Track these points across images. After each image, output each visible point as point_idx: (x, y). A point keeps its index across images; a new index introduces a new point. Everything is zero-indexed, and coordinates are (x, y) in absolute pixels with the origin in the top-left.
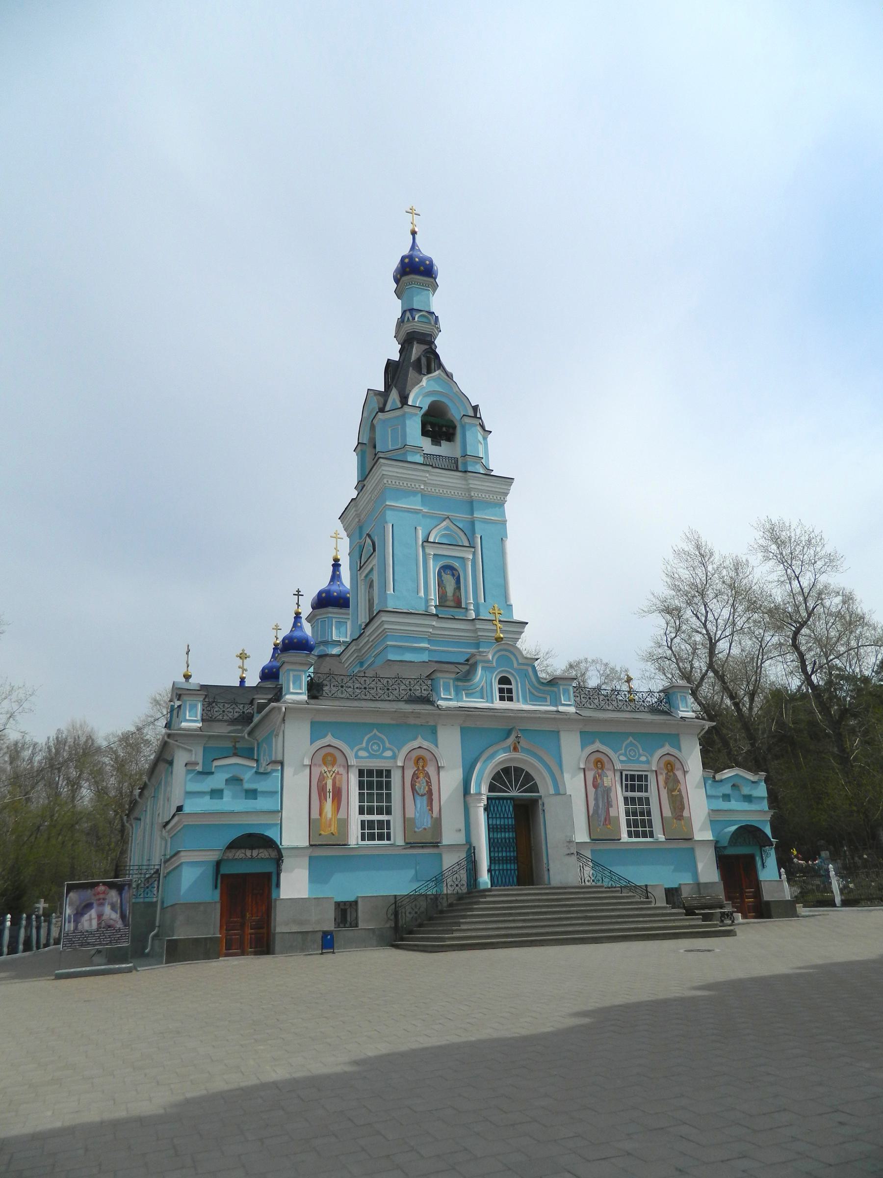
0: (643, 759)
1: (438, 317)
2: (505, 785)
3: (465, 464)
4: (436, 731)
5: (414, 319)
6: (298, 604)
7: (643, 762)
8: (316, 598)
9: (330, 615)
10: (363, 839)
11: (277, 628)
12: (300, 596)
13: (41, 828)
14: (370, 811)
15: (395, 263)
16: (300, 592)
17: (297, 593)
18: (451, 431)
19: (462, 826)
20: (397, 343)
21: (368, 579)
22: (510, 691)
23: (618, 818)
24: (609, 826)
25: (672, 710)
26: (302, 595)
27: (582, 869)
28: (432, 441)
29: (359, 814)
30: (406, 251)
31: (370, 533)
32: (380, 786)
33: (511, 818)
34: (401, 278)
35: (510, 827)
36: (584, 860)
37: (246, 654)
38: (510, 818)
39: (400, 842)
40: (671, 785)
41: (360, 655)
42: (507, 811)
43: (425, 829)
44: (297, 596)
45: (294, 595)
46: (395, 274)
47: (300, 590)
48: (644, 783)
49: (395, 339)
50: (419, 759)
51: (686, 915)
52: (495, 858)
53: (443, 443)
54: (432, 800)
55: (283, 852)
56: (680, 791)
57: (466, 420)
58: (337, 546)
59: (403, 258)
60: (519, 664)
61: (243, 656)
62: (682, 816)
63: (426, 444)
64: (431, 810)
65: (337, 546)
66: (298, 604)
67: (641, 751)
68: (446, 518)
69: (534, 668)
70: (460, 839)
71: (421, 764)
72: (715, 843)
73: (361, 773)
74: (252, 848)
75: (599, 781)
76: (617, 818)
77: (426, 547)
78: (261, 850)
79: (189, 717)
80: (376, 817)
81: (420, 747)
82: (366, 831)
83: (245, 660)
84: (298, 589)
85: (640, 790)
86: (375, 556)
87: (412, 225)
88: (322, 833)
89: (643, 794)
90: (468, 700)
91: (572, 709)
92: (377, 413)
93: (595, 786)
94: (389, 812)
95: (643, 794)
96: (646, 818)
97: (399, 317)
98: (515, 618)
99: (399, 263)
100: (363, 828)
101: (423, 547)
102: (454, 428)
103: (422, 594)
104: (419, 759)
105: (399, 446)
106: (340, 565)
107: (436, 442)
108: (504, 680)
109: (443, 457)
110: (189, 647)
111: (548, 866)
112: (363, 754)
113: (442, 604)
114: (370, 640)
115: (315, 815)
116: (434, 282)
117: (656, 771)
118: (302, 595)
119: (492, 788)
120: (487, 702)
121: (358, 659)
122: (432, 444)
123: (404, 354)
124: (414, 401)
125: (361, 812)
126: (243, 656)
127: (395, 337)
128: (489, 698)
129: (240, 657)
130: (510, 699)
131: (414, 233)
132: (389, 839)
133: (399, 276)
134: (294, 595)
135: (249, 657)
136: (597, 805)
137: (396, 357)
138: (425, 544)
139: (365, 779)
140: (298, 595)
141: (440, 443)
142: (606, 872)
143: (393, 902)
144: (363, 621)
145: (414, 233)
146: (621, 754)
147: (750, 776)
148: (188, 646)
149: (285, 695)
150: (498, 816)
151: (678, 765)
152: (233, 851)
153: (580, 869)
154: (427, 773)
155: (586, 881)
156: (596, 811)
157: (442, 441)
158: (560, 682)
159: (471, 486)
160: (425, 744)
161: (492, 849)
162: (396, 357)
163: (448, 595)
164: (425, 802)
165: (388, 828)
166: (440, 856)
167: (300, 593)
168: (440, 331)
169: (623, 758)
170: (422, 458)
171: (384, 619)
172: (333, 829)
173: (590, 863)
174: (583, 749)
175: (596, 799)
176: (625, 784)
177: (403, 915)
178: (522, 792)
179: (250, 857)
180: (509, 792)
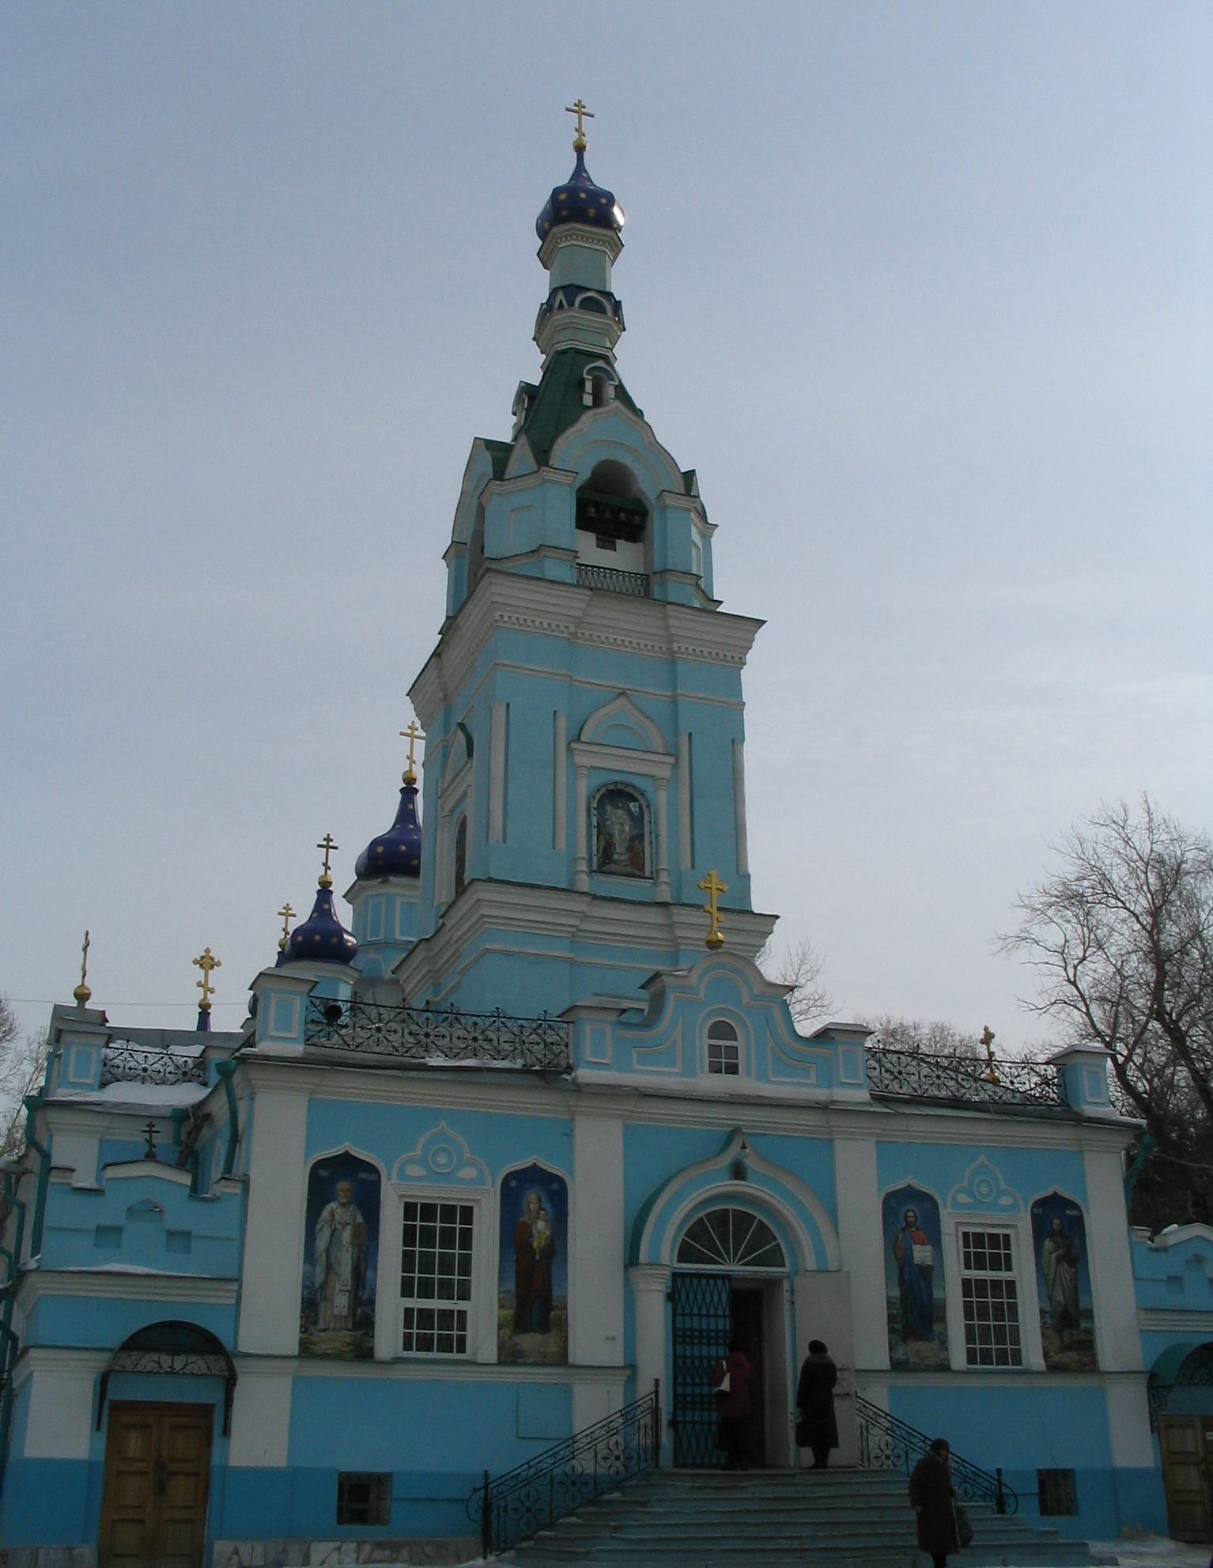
1: (620, 302)
2: (718, 1252)
4: (572, 1130)
6: (325, 864)
8: (366, 854)
10: (407, 1346)
11: (287, 913)
12: (330, 850)
14: (426, 1292)
15: (540, 201)
16: (332, 840)
19: (618, 1331)
20: (539, 350)
21: (457, 813)
22: (733, 1052)
26: (336, 848)
27: (865, 1433)
28: (597, 539)
29: (402, 1296)
30: (563, 180)
31: (465, 722)
32: (448, 1239)
33: (724, 1316)
34: (550, 228)
35: (721, 1334)
36: (871, 1413)
37: (212, 959)
38: (722, 1316)
42: (708, 1301)
44: (325, 849)
46: (539, 221)
47: (331, 837)
48: (1002, 1251)
49: (535, 343)
52: (685, 1399)
53: (620, 543)
55: (237, 1363)
57: (670, 500)
58: (411, 752)
59: (556, 192)
61: (207, 962)
63: (587, 546)
65: (411, 752)
67: (1003, 1185)
68: (621, 694)
69: (785, 1006)
74: (174, 1351)
77: (574, 752)
78: (193, 1358)
80: (435, 1304)
82: (415, 1331)
83: (210, 972)
84: (328, 835)
85: (996, 1267)
86: (471, 767)
87: (577, 133)
89: (1002, 1275)
90: (643, 1068)
92: (490, 480)
94: (465, 1295)
95: (1002, 1275)
96: (1007, 1323)
97: (545, 301)
99: (548, 202)
100: (408, 1323)
107: (606, 540)
108: (722, 1030)
109: (618, 571)
110: (89, 937)
112: (414, 1170)
114: (454, 939)
116: (615, 237)
118: (336, 848)
119: (685, 1254)
121: (430, 978)
122: (598, 546)
123: (548, 374)
125: (407, 1290)
126: (207, 962)
127: (534, 339)
129: (201, 965)
130: (733, 1069)
131: (580, 149)
132: (462, 1348)
133: (546, 225)
135: (218, 964)
137: (535, 378)
138: (574, 746)
139: (418, 1223)
141: (614, 544)
142: (914, 1440)
143: (482, 1485)
144: (443, 900)
145: (580, 149)
146: (411, 1161)
148: (87, 934)
149: (261, 1039)
150: (695, 1311)
152: (135, 1355)
153: (861, 1433)
155: (872, 1459)
157: (618, 541)
158: (838, 1037)
159: (673, 631)
161: (680, 1380)
162: (535, 378)
165: (462, 1326)
166: (568, 1390)
168: (624, 329)
170: (575, 573)
171: (482, 895)
173: (882, 1420)
176: (965, 1252)
177: (502, 1514)
179: (169, 1370)
180: (721, 1264)
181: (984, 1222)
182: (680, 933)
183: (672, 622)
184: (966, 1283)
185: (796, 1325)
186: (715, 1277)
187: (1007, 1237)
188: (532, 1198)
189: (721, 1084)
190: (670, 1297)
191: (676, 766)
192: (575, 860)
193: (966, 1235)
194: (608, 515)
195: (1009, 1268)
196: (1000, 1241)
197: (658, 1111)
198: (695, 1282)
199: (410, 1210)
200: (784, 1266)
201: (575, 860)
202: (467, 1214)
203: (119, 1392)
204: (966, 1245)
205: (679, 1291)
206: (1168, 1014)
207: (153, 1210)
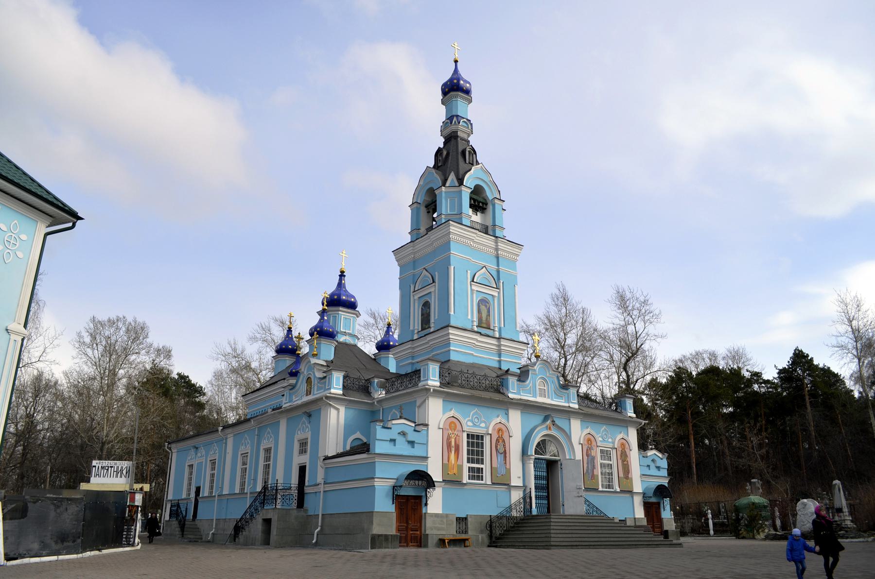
3: (494, 231)
5: (459, 123)
9: (340, 313)
10: (469, 479)
13: (771, 499)
18: (485, 206)
19: (521, 475)
23: (598, 476)
25: (623, 411)
39: (489, 482)
40: (623, 457)
41: (413, 351)
43: (502, 475)
46: (443, 87)
50: (499, 430)
54: (506, 457)
56: (627, 462)
62: (628, 477)
64: (506, 463)
71: (501, 433)
72: (644, 495)
73: (468, 435)
75: (589, 452)
79: (336, 385)
81: (453, 417)
88: (449, 473)
91: (576, 406)
93: (588, 455)
98: (2, 248)
101: (471, 285)
102: (486, 204)
103: (469, 317)
104: (499, 430)
105: (455, 213)
106: (345, 276)
113: (480, 325)
115: (446, 462)
117: (443, 429)
120: (533, 397)
124: (466, 183)
128: (534, 394)
131: (456, 62)
137: (442, 146)
145: (456, 62)
146: (468, 421)
147: (660, 455)
151: (627, 446)
154: (504, 439)
156: (587, 471)
160: (503, 421)
163: (483, 319)
164: (502, 458)
172: (455, 471)
174: (444, 414)
175: (588, 463)
178: (552, 456)
182: (502, 348)
183: (499, 244)
184: (601, 464)
185: (428, 502)
188: (500, 431)
191: (499, 293)
192: (473, 321)
194: (477, 204)
200: (601, 450)
201: (473, 321)
203: (403, 492)
206: (392, 333)
207: (403, 434)
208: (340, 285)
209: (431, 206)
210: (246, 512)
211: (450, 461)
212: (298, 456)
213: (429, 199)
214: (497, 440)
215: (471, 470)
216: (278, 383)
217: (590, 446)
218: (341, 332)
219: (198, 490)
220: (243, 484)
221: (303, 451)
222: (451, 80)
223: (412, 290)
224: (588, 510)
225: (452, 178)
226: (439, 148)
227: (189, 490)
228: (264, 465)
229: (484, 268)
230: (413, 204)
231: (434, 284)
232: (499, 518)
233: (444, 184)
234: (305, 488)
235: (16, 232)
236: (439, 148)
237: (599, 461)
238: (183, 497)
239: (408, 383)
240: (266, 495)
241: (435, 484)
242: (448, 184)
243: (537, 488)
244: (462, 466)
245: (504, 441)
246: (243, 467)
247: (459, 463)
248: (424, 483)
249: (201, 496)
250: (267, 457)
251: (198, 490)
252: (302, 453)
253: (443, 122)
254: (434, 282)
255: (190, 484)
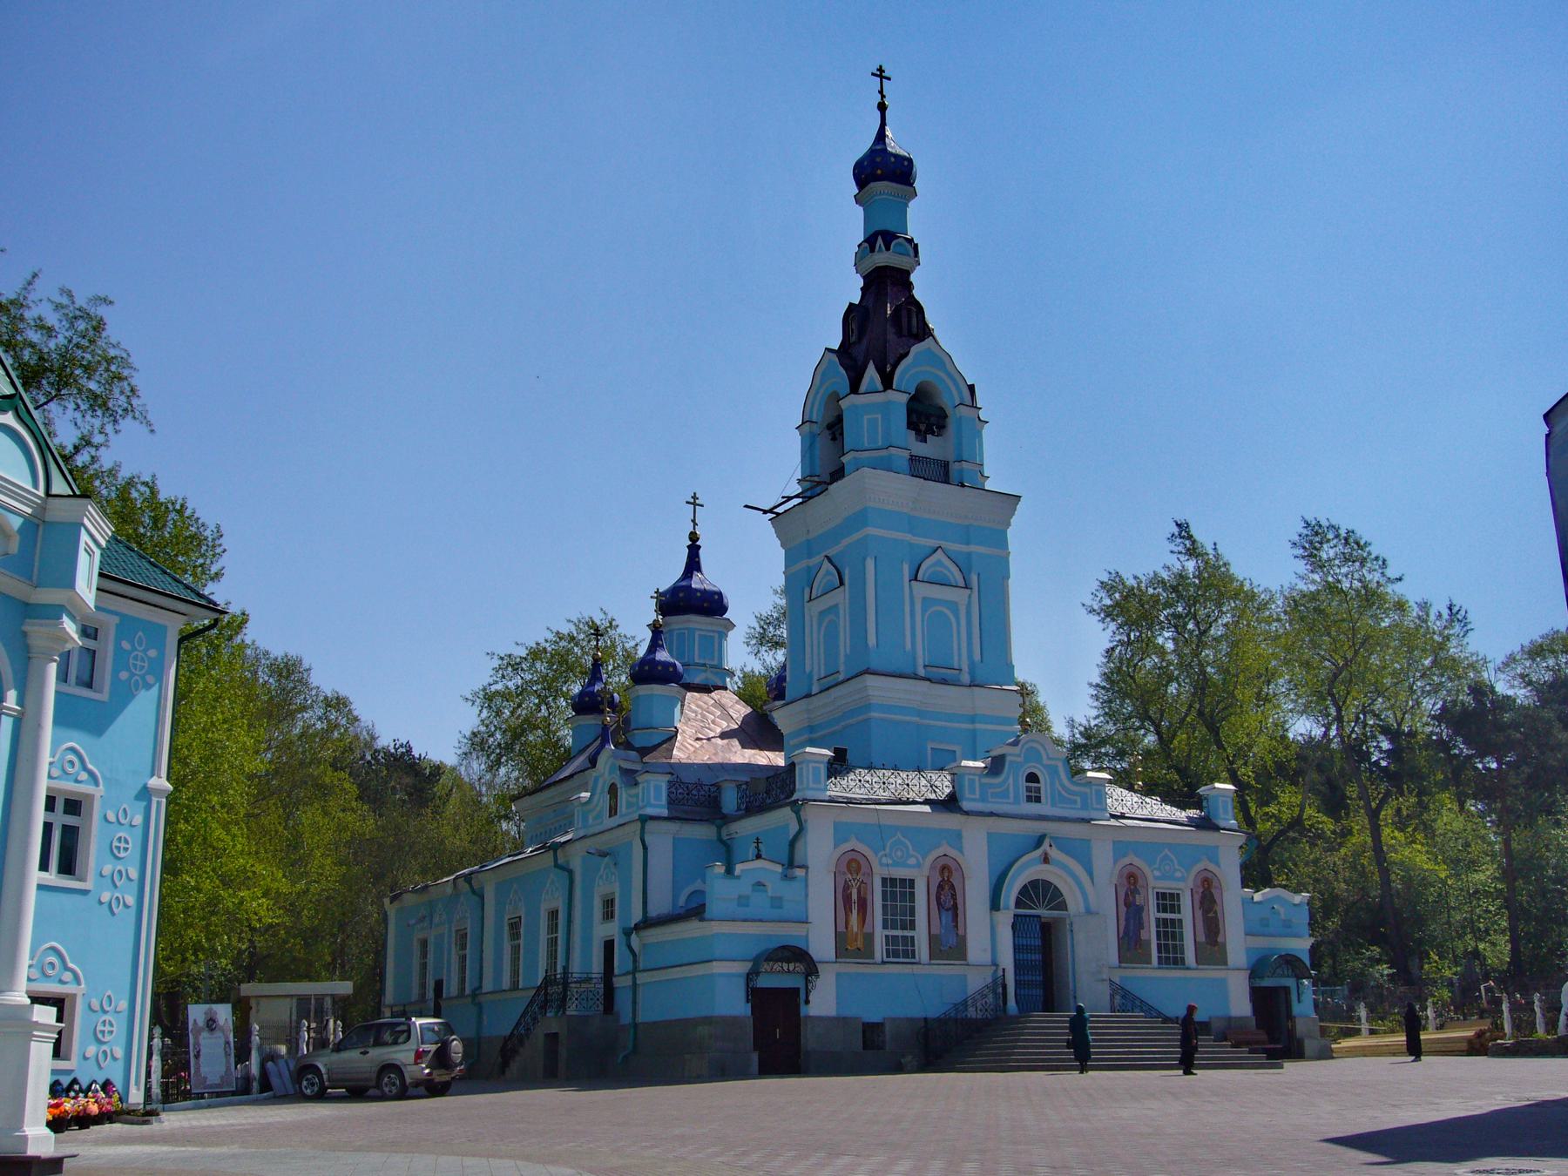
0: (1178, 874)
6: (694, 521)
7: (1178, 879)
12: (697, 507)
17: (692, 501)
24: (1140, 951)
26: (702, 506)
45: (687, 503)
50: (944, 868)
51: (1268, 1059)
56: (1216, 912)
60: (1049, 758)
62: (1216, 941)
64: (956, 926)
66: (694, 521)
70: (987, 958)
71: (946, 874)
76: (1148, 942)
80: (899, 933)
84: (695, 494)
111: (1075, 993)
115: (841, 928)
125: (885, 927)
130: (1038, 800)
134: (687, 503)
136: (1126, 927)
140: (695, 504)
164: (950, 918)
167: (697, 502)
169: (1157, 873)
172: (860, 944)
175: (1127, 919)
181: (1166, 886)
184: (1158, 920)
186: (1034, 916)
187: (1178, 894)
189: (1033, 808)
190: (1014, 926)
193: (1157, 893)
195: (1179, 912)
196: (1175, 897)
197: (908, 634)
198: (1028, 919)
199: (884, 880)
202: (912, 882)
203: (764, 982)
204: (1158, 899)
205: (1018, 924)
208: (693, 564)
209: (835, 428)
210: (518, 1024)
211: (849, 929)
212: (602, 924)
213: (830, 418)
214: (940, 887)
215: (1175, 908)
216: (575, 777)
217: (1132, 887)
218: (697, 664)
219: (439, 986)
220: (515, 973)
221: (608, 915)
222: (872, 152)
223: (807, 597)
224: (1123, 1004)
225: (871, 375)
226: (851, 304)
227: (423, 985)
228: (548, 939)
229: (940, 550)
230: (803, 423)
231: (842, 588)
232: (942, 1021)
233: (854, 389)
234: (614, 979)
235: (134, 678)
236: (851, 304)
237: (1152, 914)
238: (413, 1000)
239: (779, 791)
240: (553, 992)
241: (819, 966)
242: (863, 388)
243: (1018, 966)
244: (872, 934)
245: (952, 887)
246: (556, 935)
247: (867, 929)
248: (800, 967)
249: (444, 995)
250: (607, 912)
251: (439, 986)
252: (607, 918)
253: (859, 246)
254: (842, 583)
255: (423, 975)
